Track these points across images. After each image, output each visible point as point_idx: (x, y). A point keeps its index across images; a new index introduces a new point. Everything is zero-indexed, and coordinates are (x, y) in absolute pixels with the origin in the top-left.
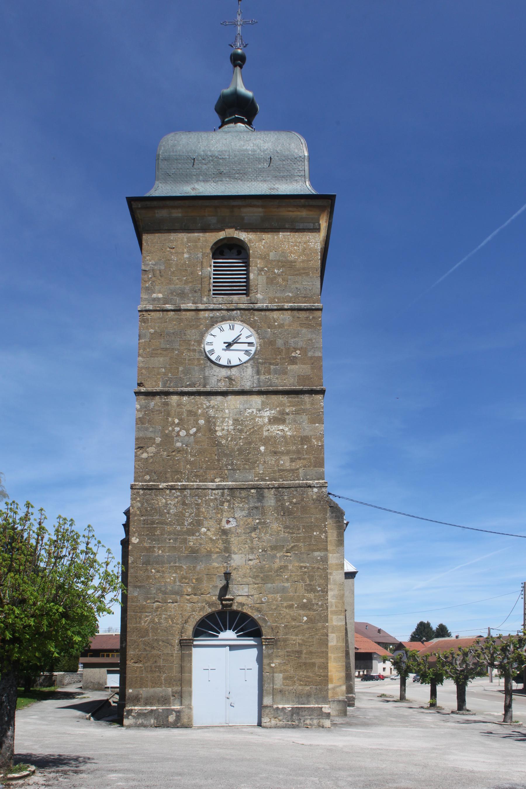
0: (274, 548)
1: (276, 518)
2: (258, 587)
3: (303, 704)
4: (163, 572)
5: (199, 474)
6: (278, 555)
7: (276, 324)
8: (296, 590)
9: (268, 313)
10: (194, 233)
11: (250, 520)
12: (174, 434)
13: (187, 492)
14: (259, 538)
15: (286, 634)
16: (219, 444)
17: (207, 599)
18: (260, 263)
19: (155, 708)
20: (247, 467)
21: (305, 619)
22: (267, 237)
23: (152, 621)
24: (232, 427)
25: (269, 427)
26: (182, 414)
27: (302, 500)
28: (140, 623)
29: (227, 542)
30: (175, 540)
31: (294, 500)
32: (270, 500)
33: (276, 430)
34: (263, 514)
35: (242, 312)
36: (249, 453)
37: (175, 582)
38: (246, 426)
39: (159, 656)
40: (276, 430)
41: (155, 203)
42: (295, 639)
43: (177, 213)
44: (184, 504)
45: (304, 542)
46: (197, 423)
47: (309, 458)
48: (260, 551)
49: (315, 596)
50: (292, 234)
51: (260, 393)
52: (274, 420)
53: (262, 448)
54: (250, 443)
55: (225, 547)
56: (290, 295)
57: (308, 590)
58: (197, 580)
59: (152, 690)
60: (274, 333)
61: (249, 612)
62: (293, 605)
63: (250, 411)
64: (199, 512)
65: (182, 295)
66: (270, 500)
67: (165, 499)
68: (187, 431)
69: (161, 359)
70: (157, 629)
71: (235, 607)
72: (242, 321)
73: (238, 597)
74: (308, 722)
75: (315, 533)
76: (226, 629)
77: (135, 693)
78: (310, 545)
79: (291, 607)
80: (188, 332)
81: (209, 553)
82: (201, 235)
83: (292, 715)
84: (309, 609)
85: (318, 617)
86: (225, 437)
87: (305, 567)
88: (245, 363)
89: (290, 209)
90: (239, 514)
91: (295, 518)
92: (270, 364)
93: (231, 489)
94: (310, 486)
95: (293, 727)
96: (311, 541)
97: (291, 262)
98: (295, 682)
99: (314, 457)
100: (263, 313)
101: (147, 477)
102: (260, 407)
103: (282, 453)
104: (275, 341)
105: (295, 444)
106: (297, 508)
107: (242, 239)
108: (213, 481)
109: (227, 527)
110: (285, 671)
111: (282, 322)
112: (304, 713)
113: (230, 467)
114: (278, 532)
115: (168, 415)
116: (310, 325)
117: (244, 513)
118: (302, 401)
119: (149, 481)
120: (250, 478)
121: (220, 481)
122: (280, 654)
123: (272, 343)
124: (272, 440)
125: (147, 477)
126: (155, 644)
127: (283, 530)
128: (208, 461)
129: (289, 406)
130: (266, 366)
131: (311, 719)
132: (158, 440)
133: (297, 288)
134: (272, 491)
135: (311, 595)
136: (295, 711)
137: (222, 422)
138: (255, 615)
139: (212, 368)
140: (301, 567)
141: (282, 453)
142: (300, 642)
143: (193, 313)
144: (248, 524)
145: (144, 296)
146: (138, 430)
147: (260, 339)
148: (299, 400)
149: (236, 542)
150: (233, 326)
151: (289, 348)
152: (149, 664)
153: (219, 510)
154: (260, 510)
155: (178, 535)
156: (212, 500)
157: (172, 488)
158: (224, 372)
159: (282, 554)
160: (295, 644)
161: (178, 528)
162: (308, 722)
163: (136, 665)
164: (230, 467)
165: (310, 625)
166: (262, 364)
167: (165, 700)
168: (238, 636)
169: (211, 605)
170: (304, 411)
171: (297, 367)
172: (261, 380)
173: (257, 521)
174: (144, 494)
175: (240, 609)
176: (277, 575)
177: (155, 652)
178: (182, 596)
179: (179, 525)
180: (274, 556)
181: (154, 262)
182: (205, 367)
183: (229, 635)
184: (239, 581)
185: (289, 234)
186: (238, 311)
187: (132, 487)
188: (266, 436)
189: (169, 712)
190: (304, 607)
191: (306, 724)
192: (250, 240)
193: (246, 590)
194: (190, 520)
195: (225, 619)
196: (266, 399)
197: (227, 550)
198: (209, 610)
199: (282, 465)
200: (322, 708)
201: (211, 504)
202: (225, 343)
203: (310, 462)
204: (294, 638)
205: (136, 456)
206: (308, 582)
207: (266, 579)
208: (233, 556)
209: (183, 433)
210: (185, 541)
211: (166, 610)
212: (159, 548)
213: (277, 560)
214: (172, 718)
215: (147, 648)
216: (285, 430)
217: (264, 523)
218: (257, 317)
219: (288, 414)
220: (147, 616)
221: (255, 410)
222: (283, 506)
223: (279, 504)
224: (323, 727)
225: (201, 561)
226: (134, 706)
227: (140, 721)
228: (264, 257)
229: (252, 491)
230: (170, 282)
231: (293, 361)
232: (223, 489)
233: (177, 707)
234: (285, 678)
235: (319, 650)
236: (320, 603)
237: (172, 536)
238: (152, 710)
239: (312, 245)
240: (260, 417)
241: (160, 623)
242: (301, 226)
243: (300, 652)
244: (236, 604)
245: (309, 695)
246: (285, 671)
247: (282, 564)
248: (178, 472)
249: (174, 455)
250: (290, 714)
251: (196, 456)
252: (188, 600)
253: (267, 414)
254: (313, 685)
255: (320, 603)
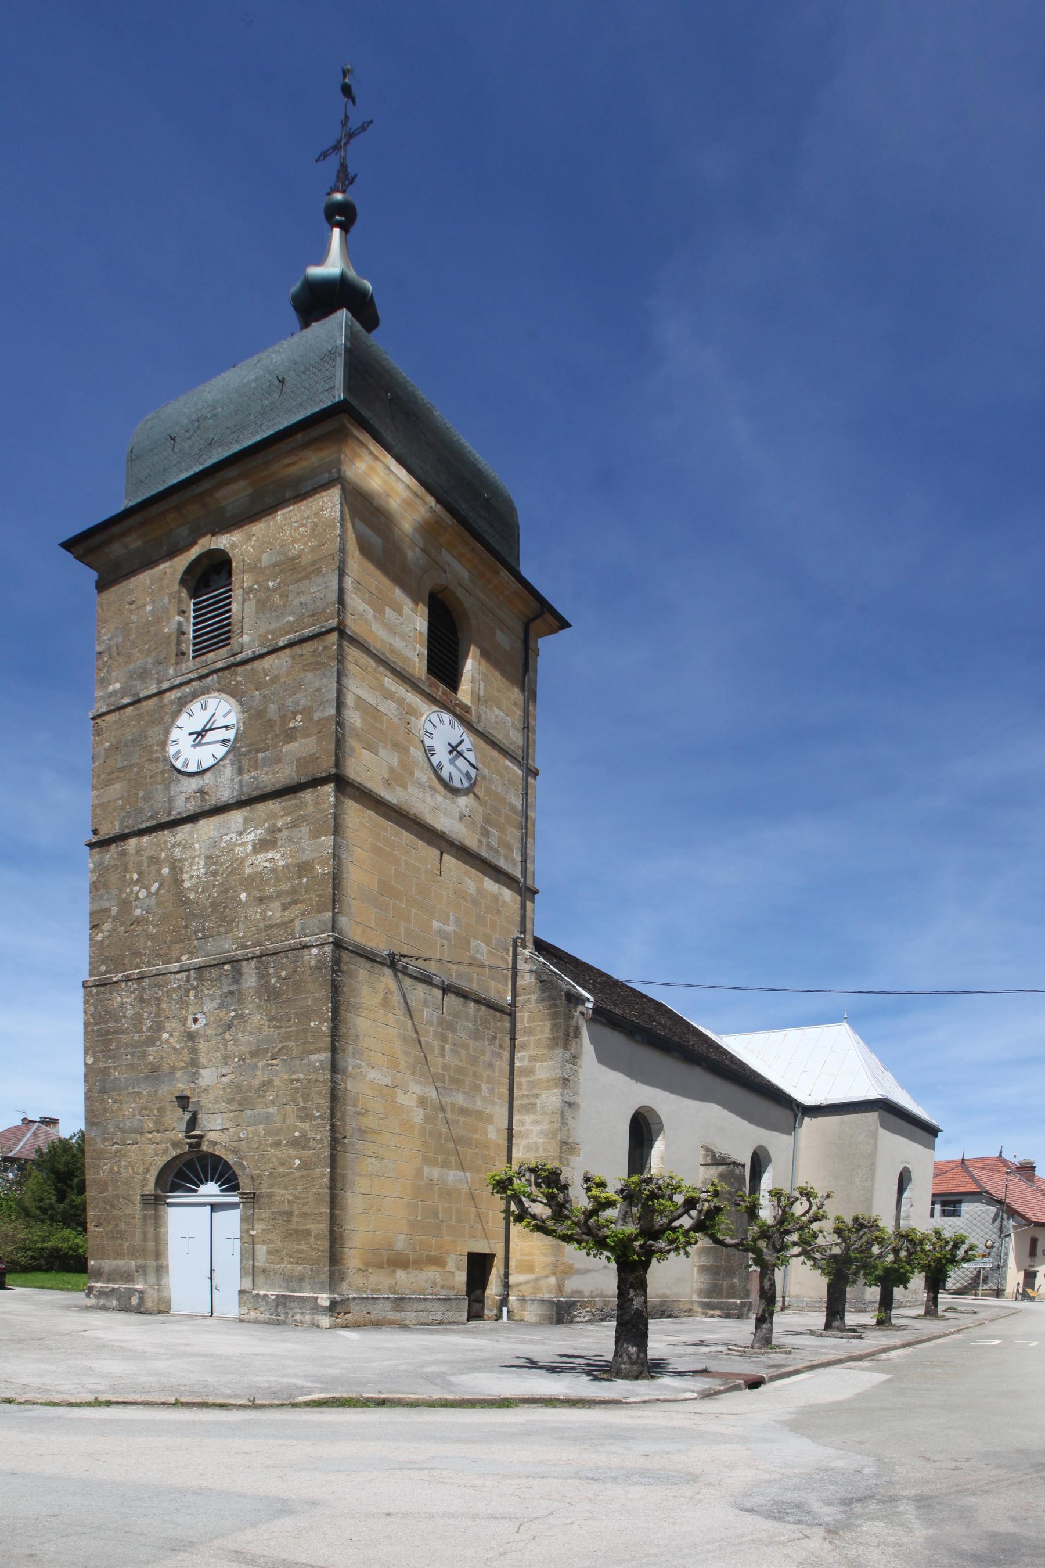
0: (255, 1054)
1: (258, 1006)
2: (235, 1116)
3: (294, 1291)
4: (121, 1102)
5: (161, 952)
6: (260, 1064)
7: (268, 678)
8: (284, 1118)
9: (256, 664)
10: (158, 565)
11: (222, 1013)
12: (132, 897)
13: (146, 982)
14: (235, 1041)
15: (272, 1186)
16: (187, 902)
17: (172, 1137)
18: (248, 580)
19: (117, 1286)
20: (222, 930)
21: (297, 1162)
22: (258, 528)
23: (111, 1170)
24: (203, 871)
25: (253, 858)
26: (142, 865)
27: (295, 971)
28: (98, 1174)
29: (194, 1051)
30: (133, 1054)
31: (283, 973)
32: (250, 980)
33: (263, 861)
34: (241, 1001)
35: (220, 674)
36: (225, 908)
37: (134, 1115)
38: (222, 864)
39: (120, 1218)
40: (263, 861)
41: (99, 539)
42: (284, 1194)
43: (135, 542)
44: (142, 1000)
45: (297, 1040)
46: (160, 874)
47: (310, 899)
48: (236, 1060)
49: (311, 1126)
50: (296, 507)
51: (241, 804)
52: (263, 845)
53: (243, 896)
54: (227, 891)
55: (191, 1058)
56: (291, 619)
57: (301, 1117)
58: (159, 1110)
59: (114, 1262)
60: (265, 697)
61: (219, 1151)
62: (281, 1141)
63: (227, 838)
64: (160, 1010)
65: (143, 675)
66: (250, 980)
67: (121, 996)
68: (148, 888)
69: (117, 786)
70: (117, 1181)
71: (205, 1148)
72: (219, 691)
73: (211, 1133)
74: (298, 1317)
75: (312, 1024)
76: (207, 1181)
77: (98, 1265)
78: (304, 1044)
79: (277, 1144)
80: (150, 733)
81: (173, 1069)
82: (168, 564)
83: (277, 1306)
84: (303, 1148)
85: (315, 1160)
86: (194, 889)
87: (297, 1081)
88: (222, 760)
89: (287, 461)
90: (209, 1006)
91: (283, 1002)
92: (258, 751)
93: (199, 969)
94: (306, 947)
95: (278, 1323)
96: (306, 1037)
97: (294, 559)
98: (282, 1259)
99: (318, 896)
100: (248, 667)
101: (103, 968)
102: (241, 828)
103: (270, 898)
104: (266, 708)
105: (289, 879)
106: (287, 985)
107: (222, 547)
108: (179, 960)
109: (194, 1027)
110: (270, 1241)
111: (276, 673)
112: (293, 1305)
113: (200, 935)
114: (260, 1028)
115: (126, 870)
116: (319, 663)
117: (215, 1004)
118: (302, 803)
119: (106, 973)
120: (225, 946)
121: (188, 959)
122: (263, 1216)
123: (260, 714)
124: (258, 879)
125: (103, 968)
126: (115, 1203)
127: (267, 1023)
128: (173, 930)
129: (282, 816)
130: (251, 756)
131: (302, 1313)
132: (115, 910)
133: (301, 604)
134: (253, 963)
135: (306, 1125)
136: (282, 1301)
137: (191, 865)
138: (231, 1159)
139: (178, 781)
140: (292, 1080)
141: (270, 898)
142: (290, 1198)
143: (155, 700)
144: (221, 1020)
145: (99, 694)
146: (93, 900)
147: (243, 712)
148: (298, 801)
149: (204, 1050)
150: (206, 702)
151: (285, 716)
152: (109, 1228)
153: (183, 1003)
154: (235, 996)
155: (136, 1047)
156: (174, 989)
157: (127, 979)
158: (194, 784)
159: (265, 1062)
160: (283, 1202)
161: (136, 1037)
162: (298, 1317)
163: (97, 1229)
164: (200, 935)
165: (304, 1172)
166: (245, 754)
167: (128, 1277)
168: (222, 1191)
169: (175, 1144)
170: (304, 819)
171: (296, 744)
172: (244, 783)
173: (233, 1014)
174: (98, 994)
175: (211, 1150)
176: (260, 1096)
177: (116, 1212)
178: (142, 1133)
179: (137, 1033)
180: (255, 1067)
181: (109, 635)
182: (170, 782)
183: (211, 1188)
184: (209, 1109)
185: (291, 508)
186: (215, 676)
187: (85, 985)
188: (249, 875)
189: (131, 1292)
190: (296, 1143)
191: (295, 1321)
192: (233, 546)
193: (219, 1121)
194: (149, 1024)
195: (193, 1167)
196: (251, 811)
197: (194, 1063)
198: (174, 1154)
199: (270, 918)
200: (317, 1298)
201: (174, 996)
202: (190, 734)
203: (311, 905)
204: (282, 1192)
205: (91, 939)
206: (302, 1105)
207: (245, 1104)
208: (202, 1071)
209: (143, 894)
210: (144, 1055)
211: (124, 1155)
212: (115, 1069)
213: (259, 1073)
214: (135, 1300)
215: (108, 1208)
216: (277, 857)
217: (242, 1016)
218: (240, 675)
219: (280, 830)
220: (106, 1164)
221: (234, 836)
222: (267, 985)
223: (263, 982)
224: (318, 1327)
225: (163, 1083)
226: (97, 1282)
227: (102, 1302)
228: (254, 568)
229: (226, 967)
230: (129, 658)
231: (290, 736)
232: (189, 970)
233: (140, 1286)
234: (270, 1252)
235: (316, 1211)
236: (318, 1137)
237: (129, 1050)
238: (113, 1289)
239: (326, 514)
240: (242, 844)
241: (119, 1173)
242: (309, 485)
243: (289, 1214)
244: (206, 1143)
245: (301, 1279)
246: (271, 1241)
247: (266, 1077)
248: (137, 954)
249: (134, 930)
250: (273, 1304)
251: (158, 925)
252: (150, 1140)
253: (251, 837)
254: (307, 1263)
255: (318, 1137)
